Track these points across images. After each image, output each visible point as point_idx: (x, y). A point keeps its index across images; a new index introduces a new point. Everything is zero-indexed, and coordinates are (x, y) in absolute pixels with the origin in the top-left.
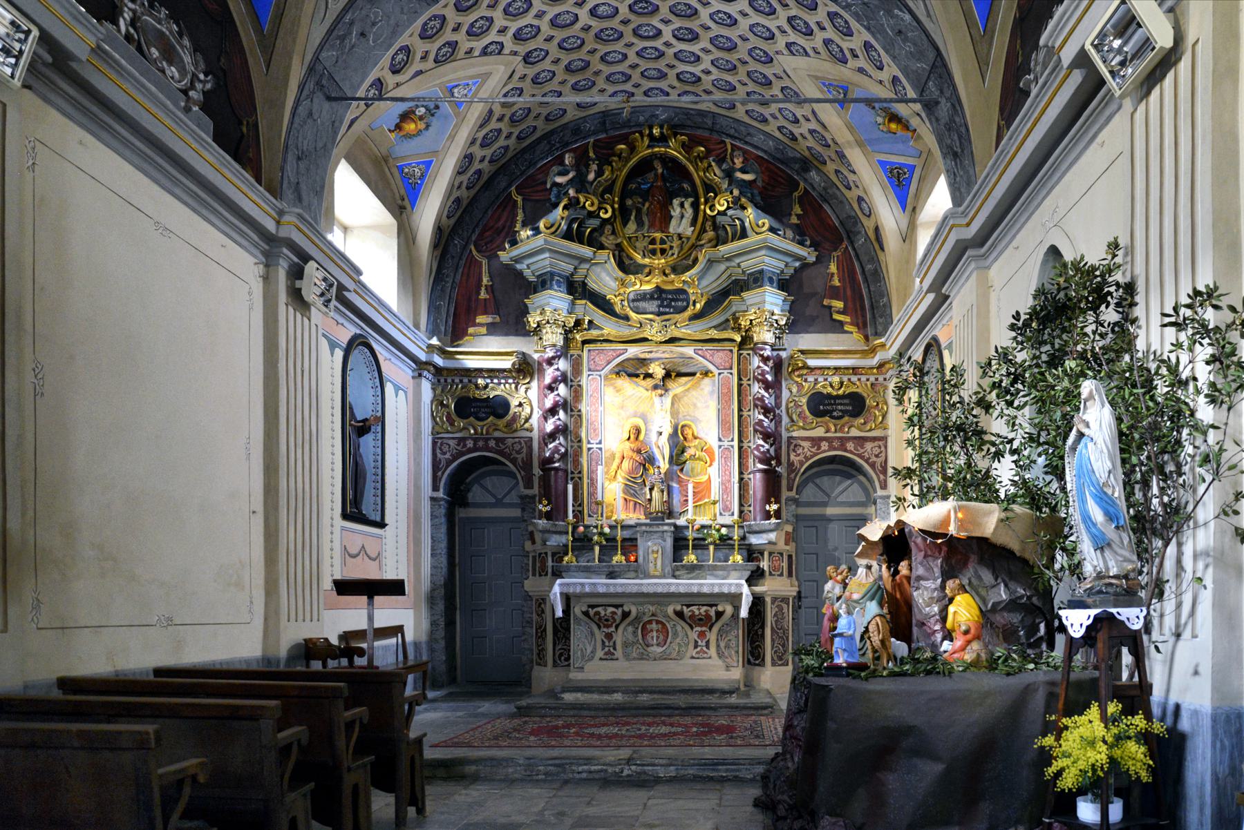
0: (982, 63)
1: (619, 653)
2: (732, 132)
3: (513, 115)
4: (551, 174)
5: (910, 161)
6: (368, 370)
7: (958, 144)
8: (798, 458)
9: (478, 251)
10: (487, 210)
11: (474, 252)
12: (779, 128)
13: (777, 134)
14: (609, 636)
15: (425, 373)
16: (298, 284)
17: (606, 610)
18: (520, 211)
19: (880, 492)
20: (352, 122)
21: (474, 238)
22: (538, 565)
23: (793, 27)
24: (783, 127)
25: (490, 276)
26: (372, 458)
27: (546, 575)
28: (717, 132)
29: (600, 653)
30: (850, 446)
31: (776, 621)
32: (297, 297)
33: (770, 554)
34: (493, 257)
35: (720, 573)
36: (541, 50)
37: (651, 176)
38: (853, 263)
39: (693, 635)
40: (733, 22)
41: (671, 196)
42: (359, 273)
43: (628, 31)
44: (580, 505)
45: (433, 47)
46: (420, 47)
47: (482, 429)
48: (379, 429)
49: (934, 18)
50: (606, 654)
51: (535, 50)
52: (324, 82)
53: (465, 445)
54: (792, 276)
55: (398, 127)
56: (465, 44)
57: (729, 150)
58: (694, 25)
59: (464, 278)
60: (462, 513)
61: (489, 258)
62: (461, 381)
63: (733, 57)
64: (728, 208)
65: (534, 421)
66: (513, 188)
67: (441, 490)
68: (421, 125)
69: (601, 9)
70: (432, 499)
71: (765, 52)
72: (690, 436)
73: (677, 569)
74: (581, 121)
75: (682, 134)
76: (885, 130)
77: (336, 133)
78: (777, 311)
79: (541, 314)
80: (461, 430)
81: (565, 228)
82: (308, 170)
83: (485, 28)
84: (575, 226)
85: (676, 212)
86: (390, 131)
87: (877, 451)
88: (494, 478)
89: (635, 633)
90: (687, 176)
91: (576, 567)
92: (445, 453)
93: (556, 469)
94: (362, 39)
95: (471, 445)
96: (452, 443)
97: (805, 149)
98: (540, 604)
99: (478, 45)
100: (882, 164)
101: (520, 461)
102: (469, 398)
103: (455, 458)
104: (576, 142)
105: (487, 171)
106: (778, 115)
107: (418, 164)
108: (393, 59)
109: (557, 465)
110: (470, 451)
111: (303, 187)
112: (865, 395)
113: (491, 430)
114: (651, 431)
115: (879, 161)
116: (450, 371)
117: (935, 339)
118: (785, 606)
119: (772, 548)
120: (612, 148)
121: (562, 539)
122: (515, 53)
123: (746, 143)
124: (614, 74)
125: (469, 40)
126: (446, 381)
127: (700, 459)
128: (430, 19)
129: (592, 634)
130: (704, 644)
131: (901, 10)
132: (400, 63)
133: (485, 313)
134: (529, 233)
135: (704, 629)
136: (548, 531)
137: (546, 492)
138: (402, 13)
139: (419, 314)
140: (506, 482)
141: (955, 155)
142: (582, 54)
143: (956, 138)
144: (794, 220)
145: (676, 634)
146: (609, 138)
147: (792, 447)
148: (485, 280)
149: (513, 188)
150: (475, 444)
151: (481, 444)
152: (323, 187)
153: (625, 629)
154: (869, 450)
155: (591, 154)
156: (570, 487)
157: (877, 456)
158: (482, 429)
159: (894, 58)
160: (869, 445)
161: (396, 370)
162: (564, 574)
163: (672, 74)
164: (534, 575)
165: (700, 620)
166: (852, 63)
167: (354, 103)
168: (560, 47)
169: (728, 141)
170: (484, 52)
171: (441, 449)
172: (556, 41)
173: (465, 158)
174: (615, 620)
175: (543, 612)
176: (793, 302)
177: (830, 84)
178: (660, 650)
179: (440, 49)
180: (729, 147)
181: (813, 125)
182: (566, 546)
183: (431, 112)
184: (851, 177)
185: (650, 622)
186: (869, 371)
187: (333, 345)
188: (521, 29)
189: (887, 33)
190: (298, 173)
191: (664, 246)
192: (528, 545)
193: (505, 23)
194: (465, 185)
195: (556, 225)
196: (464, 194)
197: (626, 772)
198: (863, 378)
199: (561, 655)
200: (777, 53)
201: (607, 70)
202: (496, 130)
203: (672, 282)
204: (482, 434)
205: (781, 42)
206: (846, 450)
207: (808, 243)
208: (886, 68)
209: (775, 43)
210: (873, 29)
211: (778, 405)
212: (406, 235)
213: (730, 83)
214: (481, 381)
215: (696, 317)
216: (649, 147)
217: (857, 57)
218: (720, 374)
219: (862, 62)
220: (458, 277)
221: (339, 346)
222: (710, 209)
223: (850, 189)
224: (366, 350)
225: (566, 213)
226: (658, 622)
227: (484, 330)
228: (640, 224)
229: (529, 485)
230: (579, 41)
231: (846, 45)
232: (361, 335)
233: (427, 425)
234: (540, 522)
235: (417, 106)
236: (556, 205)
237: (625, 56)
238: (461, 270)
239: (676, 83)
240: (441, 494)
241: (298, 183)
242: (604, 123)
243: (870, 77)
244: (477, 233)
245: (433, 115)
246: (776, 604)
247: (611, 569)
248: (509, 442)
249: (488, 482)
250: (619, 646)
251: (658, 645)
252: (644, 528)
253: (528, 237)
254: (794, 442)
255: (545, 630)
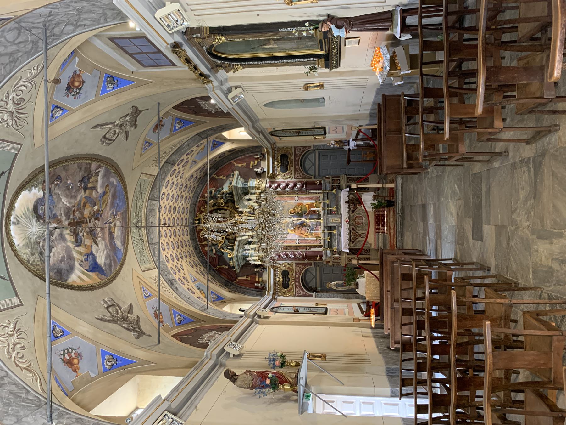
11: (235, 282)
14: (360, 235)
18: (222, 266)
19: (312, 148)
21: (231, 282)
30: (297, 159)
33: (333, 183)
53: (298, 285)
56: (182, 275)
61: (238, 277)
63: (180, 196)
66: (215, 269)
67: (312, 294)
70: (315, 297)
72: (294, 211)
73: (338, 213)
87: (299, 150)
89: (359, 227)
93: (306, 254)
96: (297, 290)
100: (212, 150)
101: (303, 267)
104: (199, 248)
110: (300, 284)
117: (269, 133)
119: (331, 183)
121: (328, 252)
127: (301, 208)
129: (359, 241)
133: (255, 278)
136: (326, 255)
144: (225, 178)
145: (359, 213)
148: (244, 278)
149: (215, 269)
151: (297, 280)
156: (312, 249)
157: (300, 150)
160: (297, 153)
164: (339, 263)
169: (199, 199)
178: (364, 219)
180: (201, 199)
185: (355, 222)
192: (330, 264)
197: (400, 215)
198: (276, 155)
199: (366, 253)
201: (182, 236)
206: (299, 160)
211: (284, 182)
214: (277, 279)
220: (243, 287)
226: (355, 219)
229: (310, 264)
239: (184, 215)
240: (314, 294)
248: (297, 270)
250: (363, 232)
251: (363, 219)
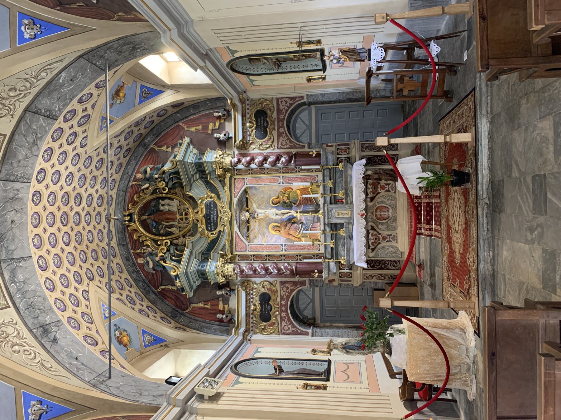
0: (85, 30)
1: (393, 233)
2: (127, 182)
3: (119, 288)
4: (149, 270)
5: (139, 87)
6: (248, 365)
7: (128, 46)
8: (288, 143)
9: (187, 309)
10: (167, 304)
11: (188, 311)
12: (124, 157)
13: (127, 158)
14: (384, 238)
15: (248, 337)
16: (206, 398)
17: (371, 239)
18: (167, 287)
20: (122, 367)
21: (180, 311)
22: (346, 278)
23: (72, 142)
24: (124, 155)
25: (199, 303)
26: (294, 365)
27: (351, 273)
28: (127, 189)
29: (393, 243)
30: (282, 117)
31: (374, 149)
32: (215, 398)
33: (338, 154)
34: (190, 301)
35: (349, 179)
36: (86, 272)
37: (149, 221)
38: (190, 120)
39: (383, 192)
40: (71, 174)
41: (158, 210)
42: (200, 365)
43: (76, 229)
44: (314, 256)
45: (84, 324)
46: (84, 331)
47: (277, 308)
48: (279, 361)
49: (62, 58)
50: (394, 240)
51: (86, 275)
52: (101, 380)
53: (285, 317)
54: (198, 149)
55: (125, 346)
57: (136, 183)
58: (73, 195)
59: (201, 316)
60: (318, 321)
61: (191, 303)
62: (252, 318)
63: (89, 177)
64: (164, 181)
65: (271, 280)
66: (156, 291)
67: (308, 331)
68: (124, 334)
69: (65, 240)
70: (312, 336)
71: (86, 160)
72: (278, 200)
73: (347, 203)
74: (122, 256)
75: (128, 206)
76: (123, 99)
77: (128, 376)
78: (215, 156)
79: (218, 275)
80: (277, 319)
81: (175, 263)
82: (146, 391)
83: (75, 298)
84: (174, 258)
85: (167, 208)
86: (127, 350)
87: (284, 103)
88: (300, 303)
89: (382, 224)
90: (149, 202)
91: (347, 256)
92: (289, 328)
93: (296, 268)
94: (78, 359)
95: (285, 313)
96: (283, 324)
97: (134, 144)
98: (367, 277)
99: (83, 302)
100: (141, 102)
102: (260, 314)
103: (291, 323)
104: (132, 259)
105: (147, 303)
106: (118, 157)
107: (144, 337)
108: (90, 344)
109: (294, 268)
110: (287, 314)
111: (155, 393)
112: (256, 110)
113: (277, 303)
114: (275, 219)
115: (139, 104)
116: (247, 324)
118: (365, 146)
120: (136, 241)
122: (88, 284)
123: (132, 175)
124: (98, 238)
125: (81, 307)
126: (252, 327)
127: (289, 194)
128: (70, 324)
129: (383, 247)
130: (387, 186)
131: (60, 78)
132: (92, 341)
133: (217, 305)
134: (178, 281)
135: (379, 186)
137: (309, 273)
138: (66, 338)
139: (219, 339)
140: (302, 297)
141: (134, 48)
142: (89, 252)
143: (125, 48)
144: (170, 149)
145: (382, 202)
146: (130, 242)
147: (283, 147)
148: (201, 305)
149: (156, 291)
150: (284, 312)
151: (283, 309)
152: (155, 383)
153: (380, 229)
154: (284, 107)
155: (139, 251)
156: (306, 261)
157: (286, 102)
158: (277, 308)
159: (86, 86)
160: (281, 107)
161: (247, 352)
162: (351, 263)
163: (98, 209)
165: (375, 188)
166: (90, 111)
167: (112, 365)
168: (85, 262)
169: (131, 183)
170: (87, 299)
171: (287, 331)
172: (82, 264)
173: (141, 313)
174: (376, 235)
175: (371, 276)
176: (210, 149)
177: (101, 127)
178: (391, 210)
179: (85, 321)
181: (122, 137)
182: (336, 263)
183: (118, 329)
184: (148, 120)
185: (376, 216)
186: (244, 108)
187: (237, 382)
188: (76, 281)
189: (72, 88)
190: (148, 396)
191: (184, 213)
192: (335, 284)
193: (73, 288)
194: (154, 315)
195: (174, 267)
196: (159, 314)
197: (487, 201)
198: (248, 111)
199: (394, 266)
200: (86, 153)
201: (96, 241)
202: (127, 297)
203: (202, 209)
204: (279, 308)
205: (80, 150)
206: (284, 119)
207: (181, 141)
208: (90, 91)
209: (81, 153)
210: (71, 97)
212: (179, 344)
213: (102, 180)
214: (252, 307)
215: (219, 197)
216: (135, 222)
217: (86, 108)
218: (247, 184)
219: (89, 105)
220: (200, 319)
221: (238, 379)
222: (165, 190)
223: (153, 121)
224: (239, 366)
225: (168, 262)
226: (376, 211)
227: (226, 306)
228: (171, 226)
230: (82, 253)
231: (80, 114)
232: (231, 368)
233: (274, 337)
234: (324, 276)
235: (115, 335)
236: (164, 267)
237: (89, 231)
238: (197, 318)
240: (310, 331)
241: (154, 396)
242: (123, 245)
243: (96, 101)
244: (178, 309)
245: (119, 328)
246: (364, 150)
247: (348, 237)
248: (282, 293)
249: (302, 307)
250: (389, 233)
251: (388, 211)
252: (326, 220)
253: (180, 282)
254: (280, 145)
255: (381, 275)
